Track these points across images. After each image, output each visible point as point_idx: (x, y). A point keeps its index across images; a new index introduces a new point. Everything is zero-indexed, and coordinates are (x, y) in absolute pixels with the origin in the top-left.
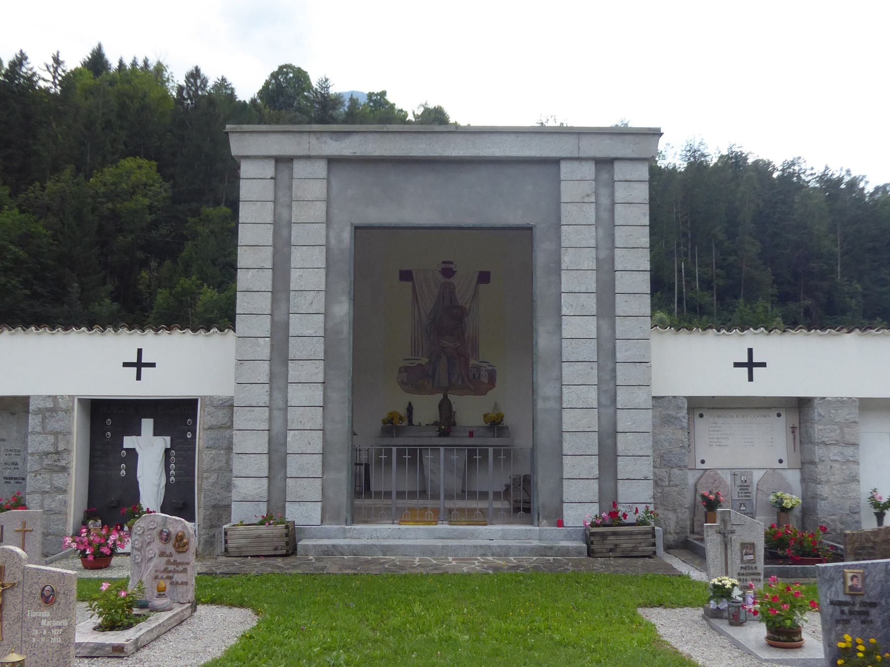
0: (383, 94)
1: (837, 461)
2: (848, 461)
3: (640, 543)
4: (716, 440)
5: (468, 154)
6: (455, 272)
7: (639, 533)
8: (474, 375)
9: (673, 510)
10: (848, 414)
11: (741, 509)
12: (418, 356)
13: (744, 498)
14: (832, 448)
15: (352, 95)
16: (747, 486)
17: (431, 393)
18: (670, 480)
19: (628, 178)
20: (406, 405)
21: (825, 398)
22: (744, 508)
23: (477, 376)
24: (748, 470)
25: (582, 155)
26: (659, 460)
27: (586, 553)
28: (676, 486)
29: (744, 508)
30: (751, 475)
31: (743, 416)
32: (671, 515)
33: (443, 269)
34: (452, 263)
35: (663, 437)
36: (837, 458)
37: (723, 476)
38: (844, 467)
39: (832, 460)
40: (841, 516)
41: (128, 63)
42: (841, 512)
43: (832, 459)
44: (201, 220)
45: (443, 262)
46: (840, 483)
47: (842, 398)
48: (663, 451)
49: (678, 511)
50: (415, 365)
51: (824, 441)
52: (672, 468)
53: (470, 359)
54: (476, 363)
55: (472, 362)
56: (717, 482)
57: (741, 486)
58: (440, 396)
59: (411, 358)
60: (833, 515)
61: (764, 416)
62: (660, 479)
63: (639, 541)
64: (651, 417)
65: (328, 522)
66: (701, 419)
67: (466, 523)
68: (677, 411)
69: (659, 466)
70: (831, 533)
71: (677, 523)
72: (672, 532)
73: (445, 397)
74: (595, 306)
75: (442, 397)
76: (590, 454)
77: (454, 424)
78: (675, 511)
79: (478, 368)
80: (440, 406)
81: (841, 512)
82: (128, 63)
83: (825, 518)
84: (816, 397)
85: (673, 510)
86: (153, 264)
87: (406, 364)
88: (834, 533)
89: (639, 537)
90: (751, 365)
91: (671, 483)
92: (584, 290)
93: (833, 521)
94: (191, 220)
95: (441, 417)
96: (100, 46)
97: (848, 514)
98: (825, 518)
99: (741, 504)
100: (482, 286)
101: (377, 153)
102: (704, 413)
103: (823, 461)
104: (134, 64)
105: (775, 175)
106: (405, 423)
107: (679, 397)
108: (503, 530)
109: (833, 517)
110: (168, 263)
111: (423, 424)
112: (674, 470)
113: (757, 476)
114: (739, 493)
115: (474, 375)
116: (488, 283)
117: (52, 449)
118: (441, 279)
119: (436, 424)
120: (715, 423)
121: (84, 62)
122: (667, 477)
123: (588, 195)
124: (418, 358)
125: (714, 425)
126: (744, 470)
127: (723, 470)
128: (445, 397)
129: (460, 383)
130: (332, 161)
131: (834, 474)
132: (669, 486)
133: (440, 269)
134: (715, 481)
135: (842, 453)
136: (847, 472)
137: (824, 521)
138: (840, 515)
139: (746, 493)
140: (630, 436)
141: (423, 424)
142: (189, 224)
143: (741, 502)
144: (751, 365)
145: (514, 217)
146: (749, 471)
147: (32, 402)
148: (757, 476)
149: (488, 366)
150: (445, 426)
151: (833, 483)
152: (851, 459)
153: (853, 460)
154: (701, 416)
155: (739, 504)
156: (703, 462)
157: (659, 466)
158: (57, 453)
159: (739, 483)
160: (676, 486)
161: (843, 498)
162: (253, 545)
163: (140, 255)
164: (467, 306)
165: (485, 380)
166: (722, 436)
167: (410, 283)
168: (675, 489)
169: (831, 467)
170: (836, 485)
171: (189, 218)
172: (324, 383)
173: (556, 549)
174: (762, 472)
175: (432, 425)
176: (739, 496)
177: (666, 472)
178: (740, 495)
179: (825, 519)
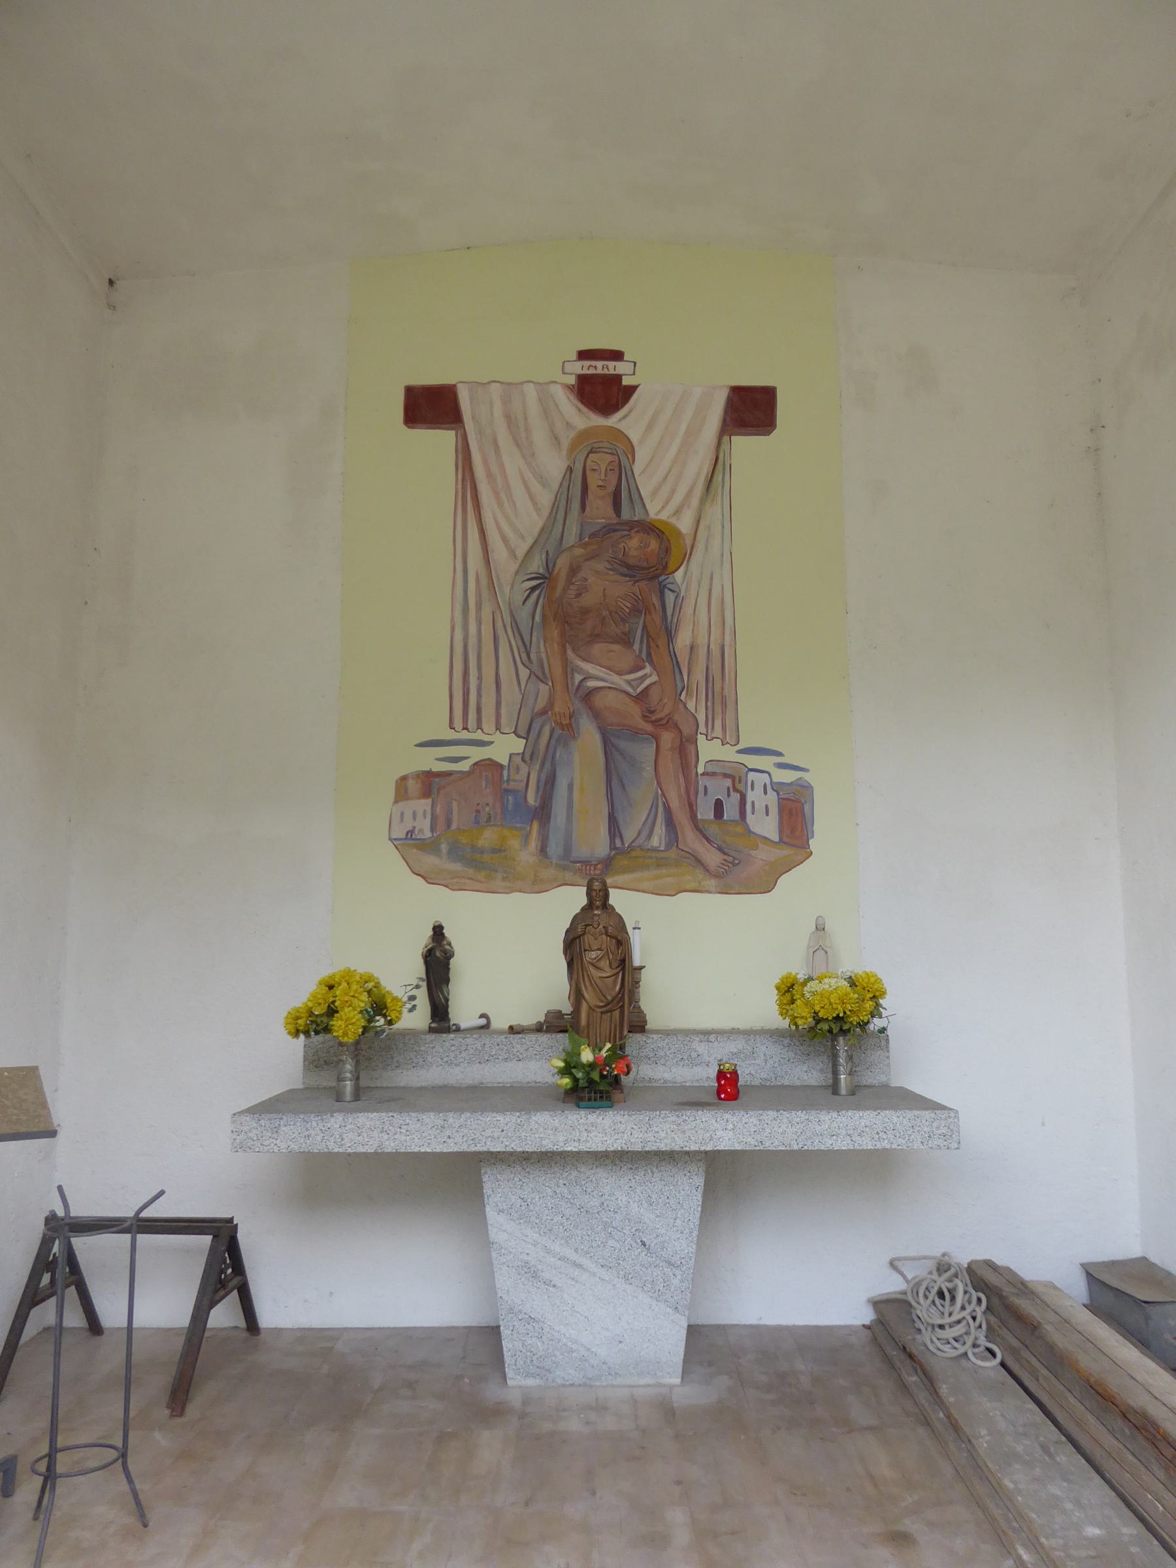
0: (778, 988)
6: (632, 390)
8: (719, 806)
12: (479, 727)
17: (538, 885)
20: (424, 937)
23: (731, 812)
33: (583, 380)
34: (617, 356)
45: (584, 355)
50: (465, 766)
53: (701, 739)
54: (728, 754)
55: (709, 751)
58: (574, 898)
59: (451, 735)
73: (598, 900)
75: (583, 901)
77: (639, 1026)
79: (736, 779)
80: (573, 944)
87: (430, 761)
95: (577, 996)
100: (743, 445)
101: (712, 610)
106: (416, 1018)
111: (500, 1022)
115: (719, 806)
116: (768, 433)
118: (582, 419)
119: (554, 1024)
124: (478, 735)
128: (598, 900)
129: (658, 838)
133: (572, 380)
141: (500, 1022)
149: (781, 766)
150: (597, 1048)
164: (684, 524)
165: (765, 825)
167: (575, 358)
175: (539, 1029)
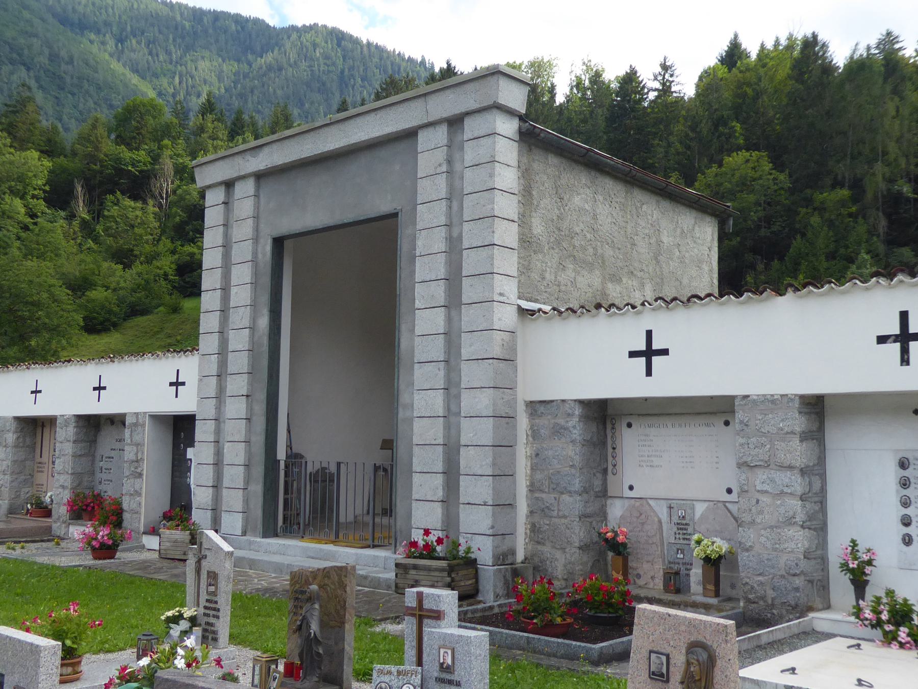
1: (766, 492)
2: (782, 492)
3: (437, 582)
4: (646, 458)
5: (342, 145)
7: (436, 570)
9: (562, 549)
10: (783, 420)
11: (678, 556)
13: (682, 541)
14: (759, 472)
15: (665, 60)
16: (686, 524)
18: (559, 510)
19: (476, 135)
21: (748, 396)
22: (682, 556)
24: (688, 502)
25: (431, 119)
26: (547, 483)
27: (394, 588)
28: (565, 517)
29: (682, 556)
30: (693, 508)
31: (680, 426)
32: (558, 554)
35: (550, 453)
36: (766, 487)
37: (656, 508)
38: (779, 502)
39: (758, 491)
40: (773, 578)
41: (770, 45)
42: (772, 571)
43: (758, 488)
44: (815, 209)
46: (771, 527)
47: (772, 395)
48: (551, 471)
49: (567, 550)
51: (746, 462)
52: (562, 493)
56: (643, 516)
57: (678, 524)
60: (760, 575)
61: (707, 425)
62: (547, 507)
63: (436, 579)
64: (491, 427)
65: (530, 547)
66: (629, 430)
67: (344, 544)
68: (568, 419)
69: (547, 490)
70: (757, 603)
71: (565, 566)
72: (560, 577)
74: (443, 294)
76: (435, 471)
78: (563, 549)
81: (772, 571)
82: (770, 45)
83: (749, 578)
84: (737, 396)
85: (562, 549)
86: (760, 267)
88: (761, 603)
89: (437, 574)
90: (649, 353)
91: (561, 513)
92: (434, 278)
93: (761, 584)
94: (803, 211)
96: (736, 36)
97: (782, 576)
98: (749, 578)
99: (678, 550)
102: (631, 421)
103: (746, 491)
104: (777, 43)
105: (560, 99)
107: (568, 400)
108: (357, 554)
109: (760, 578)
110: (776, 264)
112: (564, 496)
113: (700, 509)
114: (675, 533)
117: (134, 458)
120: (647, 435)
121: (722, 57)
122: (556, 505)
123: (440, 165)
125: (643, 438)
126: (683, 502)
127: (658, 502)
130: (260, 176)
131: (761, 512)
132: (559, 517)
134: (641, 514)
135: (772, 481)
136: (782, 510)
137: (747, 583)
138: (771, 576)
139: (684, 534)
140: (472, 450)
142: (801, 215)
143: (678, 546)
144: (649, 353)
145: (384, 206)
146: (690, 503)
147: (127, 418)
148: (700, 509)
151: (760, 526)
152: (786, 490)
153: (789, 491)
154: (629, 425)
155: (676, 550)
156: (631, 488)
157: (547, 490)
158: (137, 461)
159: (675, 519)
160: (565, 517)
161: (775, 550)
162: (173, 548)
163: (749, 257)
166: (654, 453)
168: (563, 521)
169: (758, 501)
170: (765, 529)
171: (800, 209)
172: (247, 396)
173: (370, 579)
174: (706, 505)
176: (676, 538)
177: (555, 498)
178: (677, 536)
179: (748, 580)
